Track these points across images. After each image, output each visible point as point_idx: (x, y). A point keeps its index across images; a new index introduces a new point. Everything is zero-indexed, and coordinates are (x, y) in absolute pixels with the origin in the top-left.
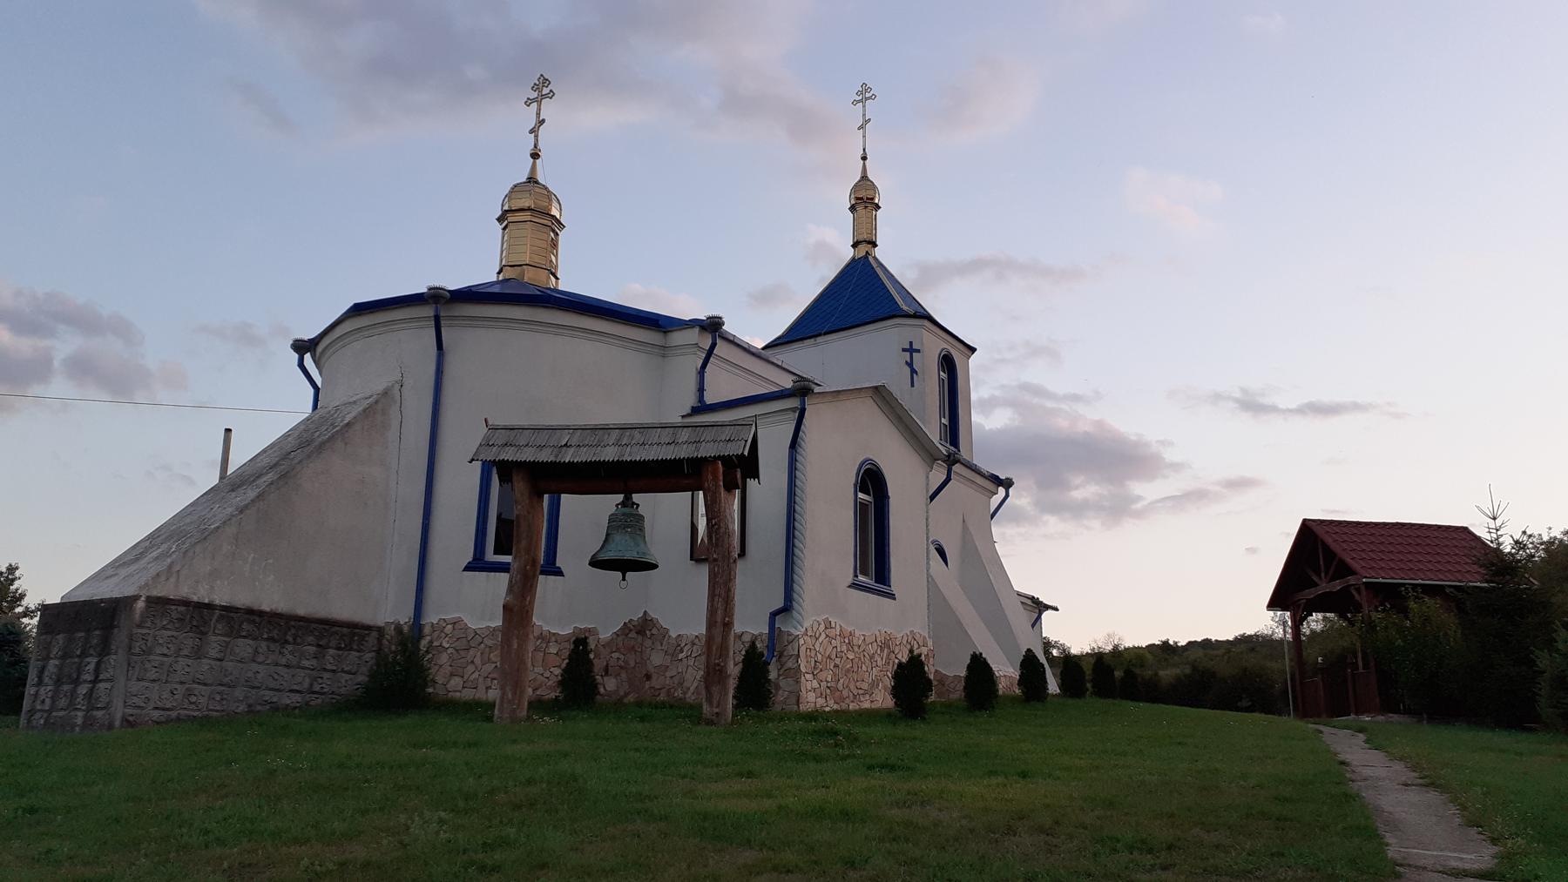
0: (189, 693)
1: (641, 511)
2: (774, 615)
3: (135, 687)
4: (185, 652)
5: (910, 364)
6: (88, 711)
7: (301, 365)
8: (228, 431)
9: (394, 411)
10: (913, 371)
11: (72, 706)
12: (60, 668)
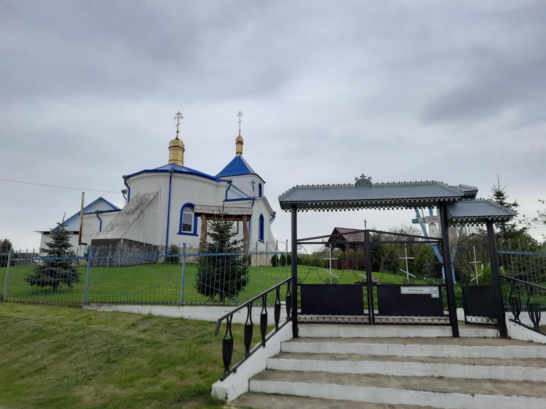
5: (253, 186)
9: (159, 197)
10: (254, 188)
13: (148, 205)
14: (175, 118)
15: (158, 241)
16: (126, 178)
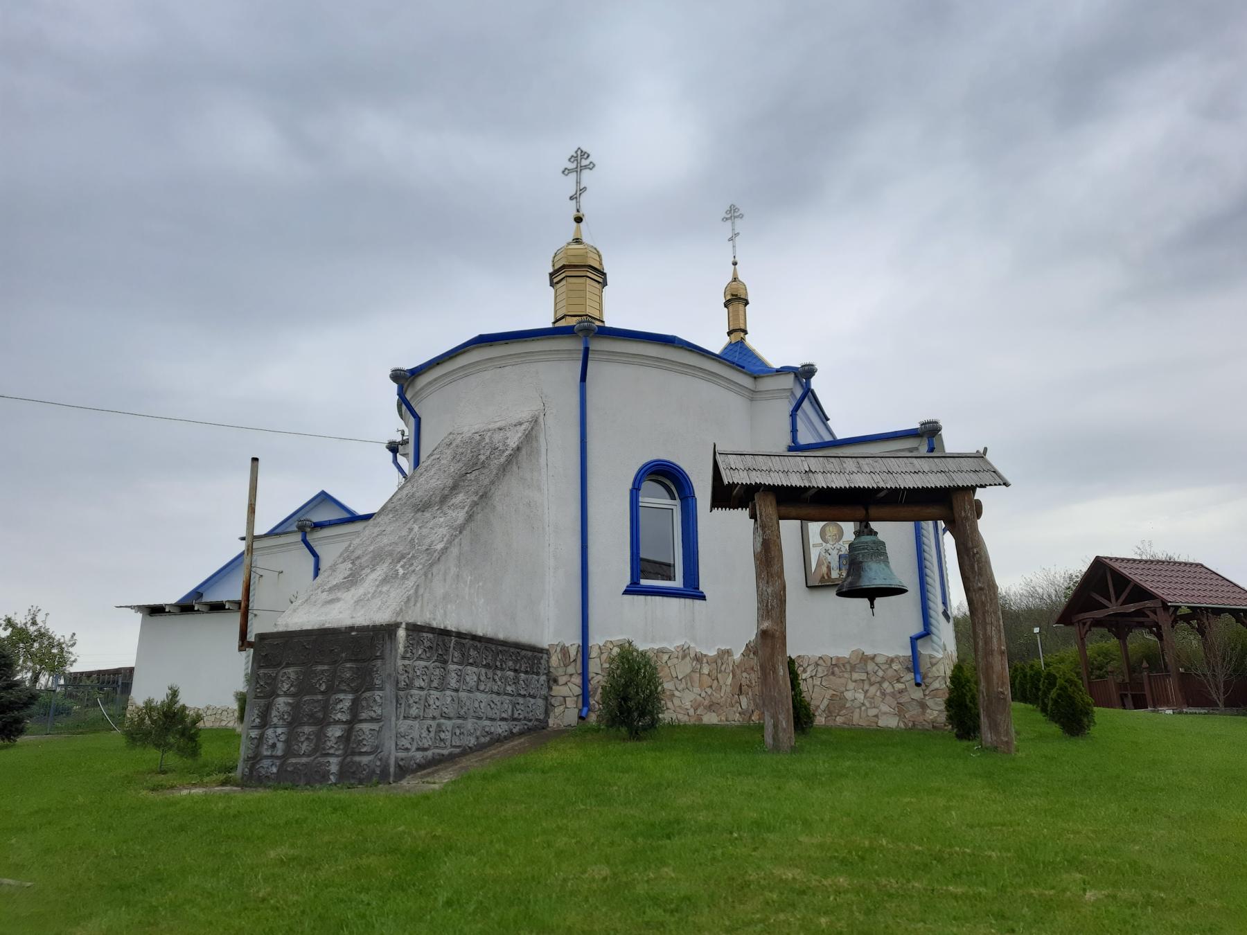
0: (440, 729)
1: (880, 537)
2: (914, 640)
3: (404, 726)
4: (435, 684)
6: (345, 755)
8: (255, 460)
11: (319, 748)
12: (296, 707)
13: (504, 469)
14: (566, 171)
15: (549, 627)
16: (404, 379)
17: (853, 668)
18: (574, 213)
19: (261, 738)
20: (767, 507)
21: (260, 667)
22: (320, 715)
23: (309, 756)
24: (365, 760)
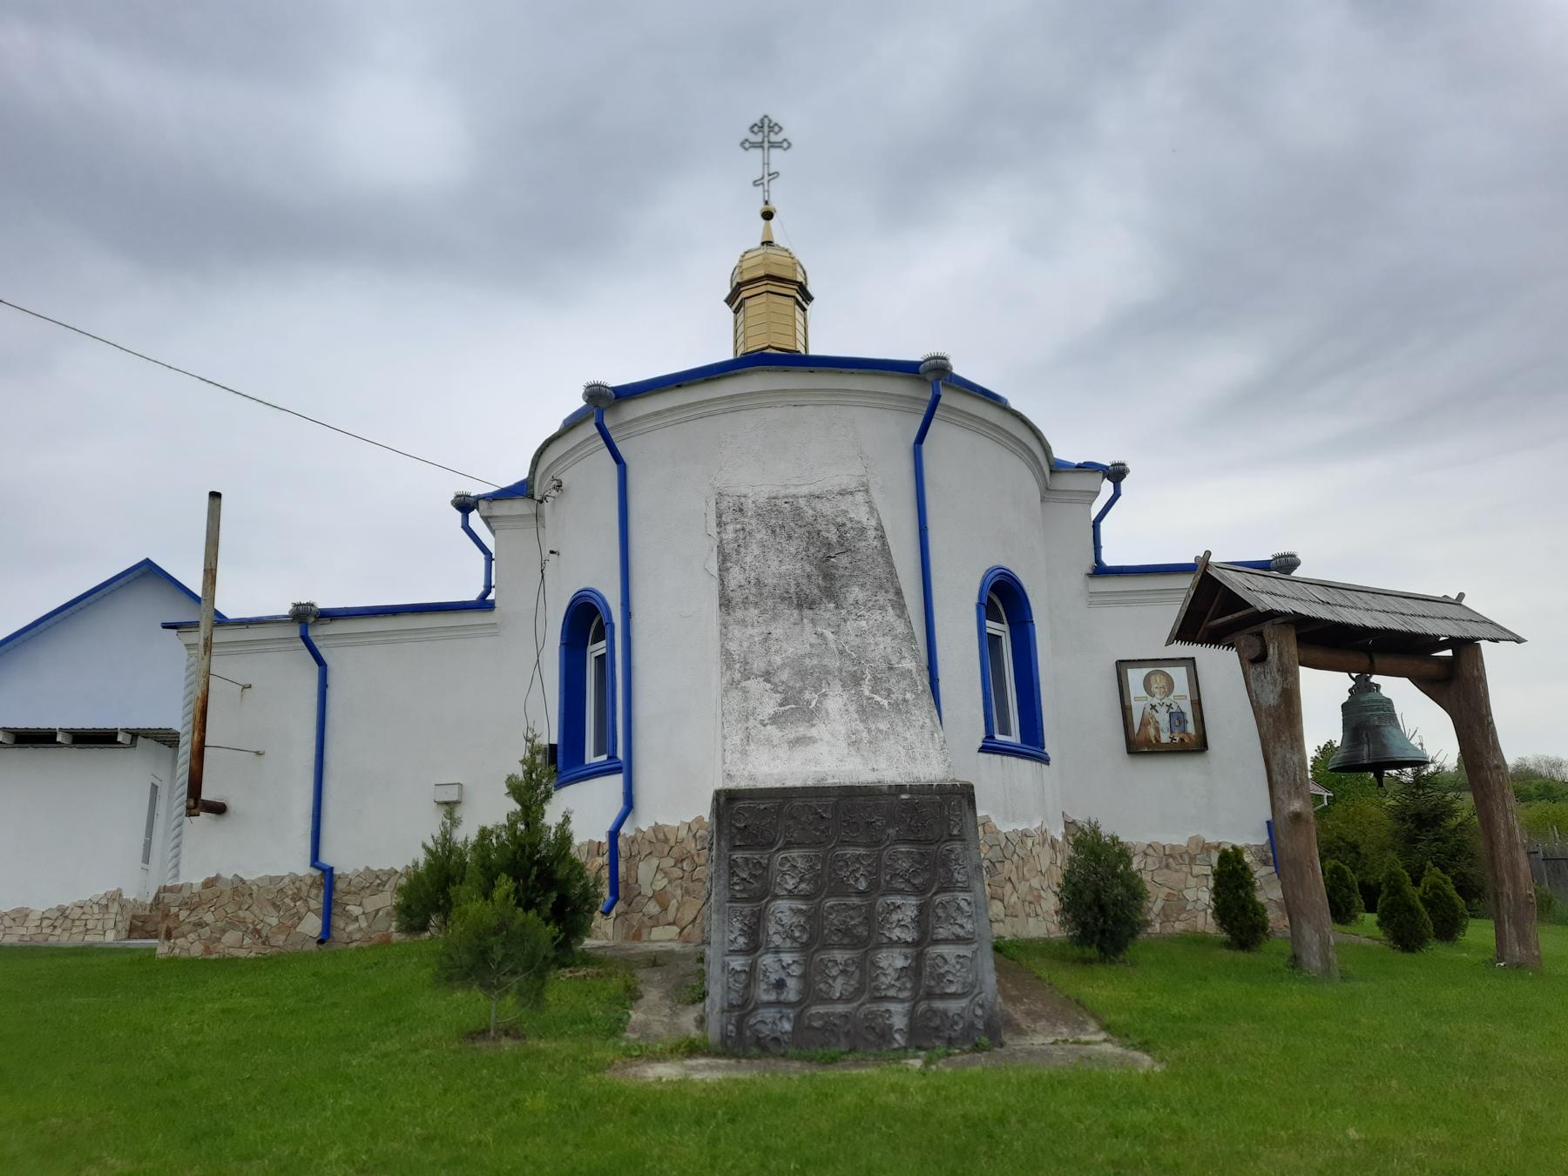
1: (1384, 692)
6: (915, 999)
7: (466, 527)
8: (215, 496)
11: (866, 984)
12: (814, 918)
17: (1193, 859)
18: (761, 207)
19: (751, 972)
20: (1281, 646)
21: (735, 848)
22: (862, 931)
23: (848, 1001)
24: (954, 1006)
